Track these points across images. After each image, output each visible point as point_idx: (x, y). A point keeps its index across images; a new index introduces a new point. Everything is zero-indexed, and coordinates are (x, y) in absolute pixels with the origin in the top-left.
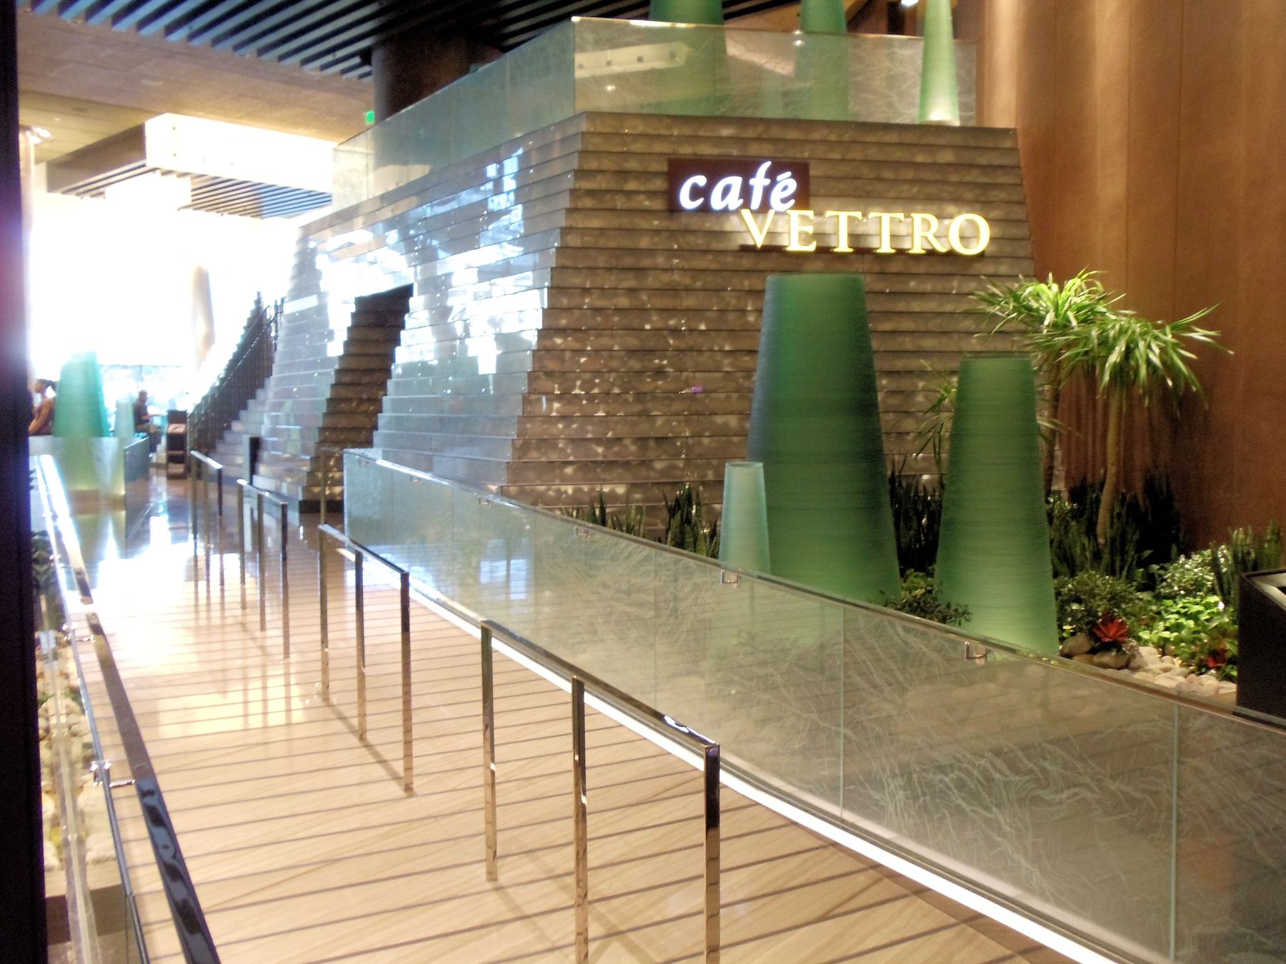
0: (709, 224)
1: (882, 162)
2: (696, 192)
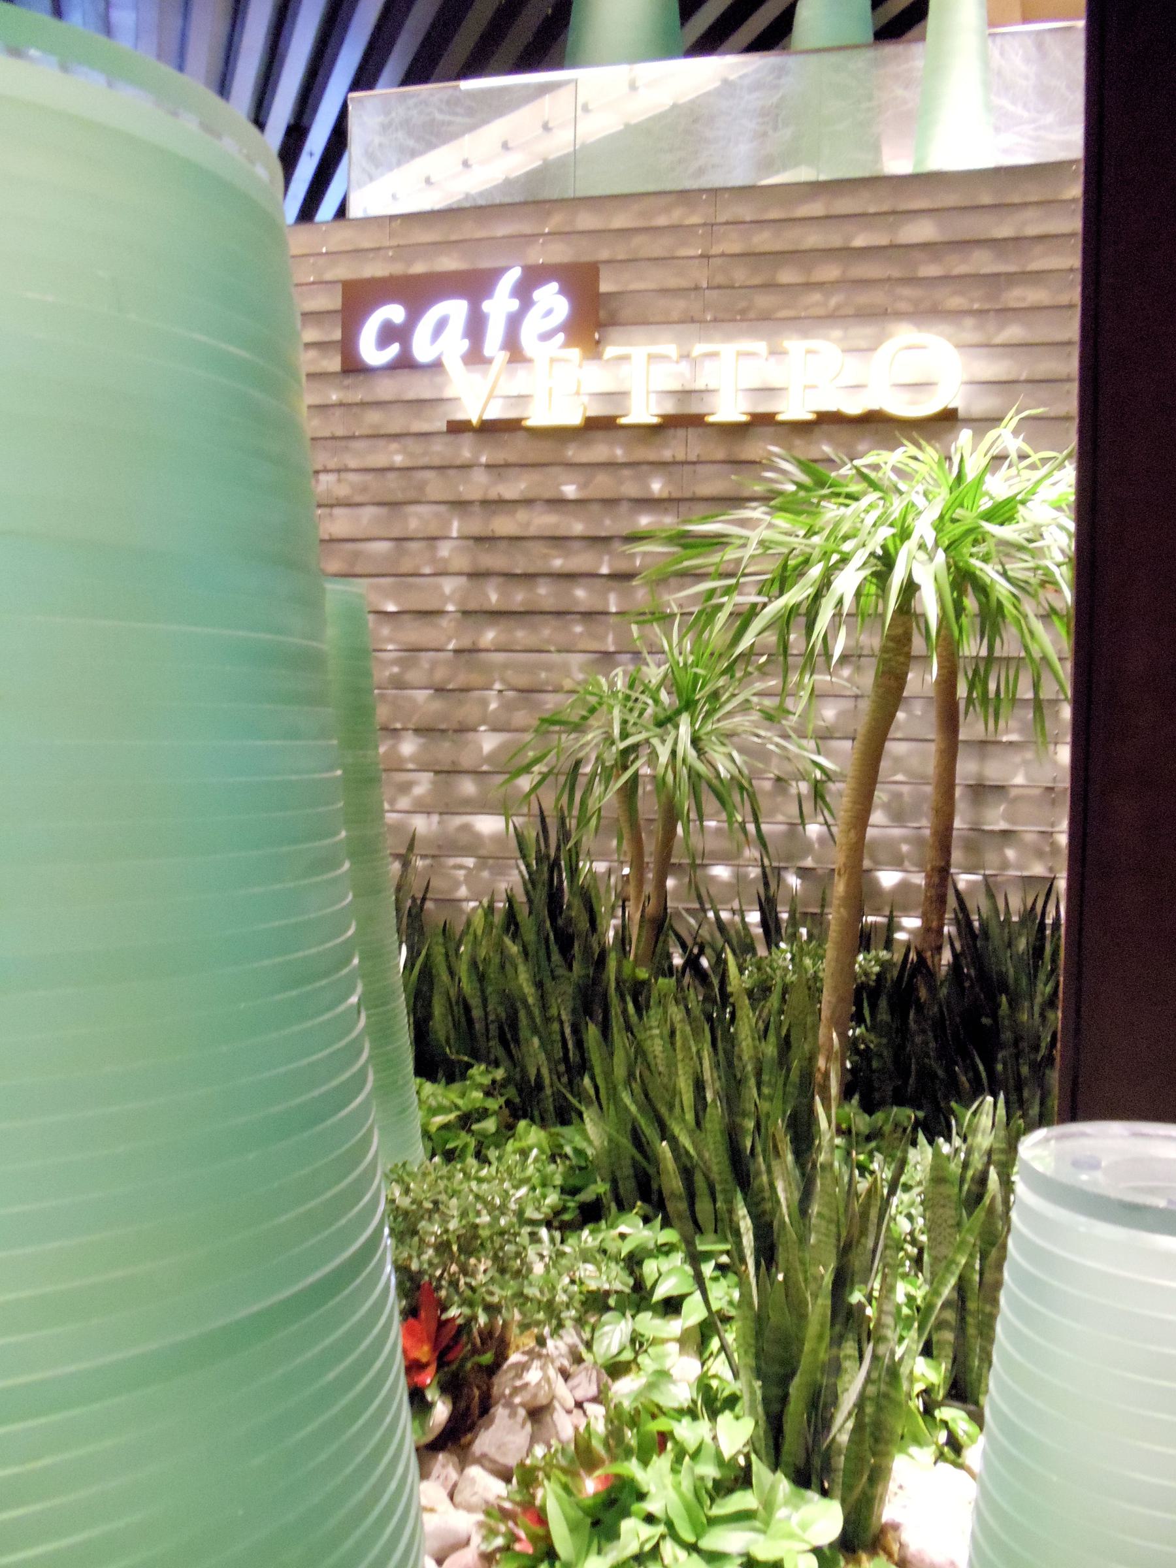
0: (417, 387)
2: (388, 334)
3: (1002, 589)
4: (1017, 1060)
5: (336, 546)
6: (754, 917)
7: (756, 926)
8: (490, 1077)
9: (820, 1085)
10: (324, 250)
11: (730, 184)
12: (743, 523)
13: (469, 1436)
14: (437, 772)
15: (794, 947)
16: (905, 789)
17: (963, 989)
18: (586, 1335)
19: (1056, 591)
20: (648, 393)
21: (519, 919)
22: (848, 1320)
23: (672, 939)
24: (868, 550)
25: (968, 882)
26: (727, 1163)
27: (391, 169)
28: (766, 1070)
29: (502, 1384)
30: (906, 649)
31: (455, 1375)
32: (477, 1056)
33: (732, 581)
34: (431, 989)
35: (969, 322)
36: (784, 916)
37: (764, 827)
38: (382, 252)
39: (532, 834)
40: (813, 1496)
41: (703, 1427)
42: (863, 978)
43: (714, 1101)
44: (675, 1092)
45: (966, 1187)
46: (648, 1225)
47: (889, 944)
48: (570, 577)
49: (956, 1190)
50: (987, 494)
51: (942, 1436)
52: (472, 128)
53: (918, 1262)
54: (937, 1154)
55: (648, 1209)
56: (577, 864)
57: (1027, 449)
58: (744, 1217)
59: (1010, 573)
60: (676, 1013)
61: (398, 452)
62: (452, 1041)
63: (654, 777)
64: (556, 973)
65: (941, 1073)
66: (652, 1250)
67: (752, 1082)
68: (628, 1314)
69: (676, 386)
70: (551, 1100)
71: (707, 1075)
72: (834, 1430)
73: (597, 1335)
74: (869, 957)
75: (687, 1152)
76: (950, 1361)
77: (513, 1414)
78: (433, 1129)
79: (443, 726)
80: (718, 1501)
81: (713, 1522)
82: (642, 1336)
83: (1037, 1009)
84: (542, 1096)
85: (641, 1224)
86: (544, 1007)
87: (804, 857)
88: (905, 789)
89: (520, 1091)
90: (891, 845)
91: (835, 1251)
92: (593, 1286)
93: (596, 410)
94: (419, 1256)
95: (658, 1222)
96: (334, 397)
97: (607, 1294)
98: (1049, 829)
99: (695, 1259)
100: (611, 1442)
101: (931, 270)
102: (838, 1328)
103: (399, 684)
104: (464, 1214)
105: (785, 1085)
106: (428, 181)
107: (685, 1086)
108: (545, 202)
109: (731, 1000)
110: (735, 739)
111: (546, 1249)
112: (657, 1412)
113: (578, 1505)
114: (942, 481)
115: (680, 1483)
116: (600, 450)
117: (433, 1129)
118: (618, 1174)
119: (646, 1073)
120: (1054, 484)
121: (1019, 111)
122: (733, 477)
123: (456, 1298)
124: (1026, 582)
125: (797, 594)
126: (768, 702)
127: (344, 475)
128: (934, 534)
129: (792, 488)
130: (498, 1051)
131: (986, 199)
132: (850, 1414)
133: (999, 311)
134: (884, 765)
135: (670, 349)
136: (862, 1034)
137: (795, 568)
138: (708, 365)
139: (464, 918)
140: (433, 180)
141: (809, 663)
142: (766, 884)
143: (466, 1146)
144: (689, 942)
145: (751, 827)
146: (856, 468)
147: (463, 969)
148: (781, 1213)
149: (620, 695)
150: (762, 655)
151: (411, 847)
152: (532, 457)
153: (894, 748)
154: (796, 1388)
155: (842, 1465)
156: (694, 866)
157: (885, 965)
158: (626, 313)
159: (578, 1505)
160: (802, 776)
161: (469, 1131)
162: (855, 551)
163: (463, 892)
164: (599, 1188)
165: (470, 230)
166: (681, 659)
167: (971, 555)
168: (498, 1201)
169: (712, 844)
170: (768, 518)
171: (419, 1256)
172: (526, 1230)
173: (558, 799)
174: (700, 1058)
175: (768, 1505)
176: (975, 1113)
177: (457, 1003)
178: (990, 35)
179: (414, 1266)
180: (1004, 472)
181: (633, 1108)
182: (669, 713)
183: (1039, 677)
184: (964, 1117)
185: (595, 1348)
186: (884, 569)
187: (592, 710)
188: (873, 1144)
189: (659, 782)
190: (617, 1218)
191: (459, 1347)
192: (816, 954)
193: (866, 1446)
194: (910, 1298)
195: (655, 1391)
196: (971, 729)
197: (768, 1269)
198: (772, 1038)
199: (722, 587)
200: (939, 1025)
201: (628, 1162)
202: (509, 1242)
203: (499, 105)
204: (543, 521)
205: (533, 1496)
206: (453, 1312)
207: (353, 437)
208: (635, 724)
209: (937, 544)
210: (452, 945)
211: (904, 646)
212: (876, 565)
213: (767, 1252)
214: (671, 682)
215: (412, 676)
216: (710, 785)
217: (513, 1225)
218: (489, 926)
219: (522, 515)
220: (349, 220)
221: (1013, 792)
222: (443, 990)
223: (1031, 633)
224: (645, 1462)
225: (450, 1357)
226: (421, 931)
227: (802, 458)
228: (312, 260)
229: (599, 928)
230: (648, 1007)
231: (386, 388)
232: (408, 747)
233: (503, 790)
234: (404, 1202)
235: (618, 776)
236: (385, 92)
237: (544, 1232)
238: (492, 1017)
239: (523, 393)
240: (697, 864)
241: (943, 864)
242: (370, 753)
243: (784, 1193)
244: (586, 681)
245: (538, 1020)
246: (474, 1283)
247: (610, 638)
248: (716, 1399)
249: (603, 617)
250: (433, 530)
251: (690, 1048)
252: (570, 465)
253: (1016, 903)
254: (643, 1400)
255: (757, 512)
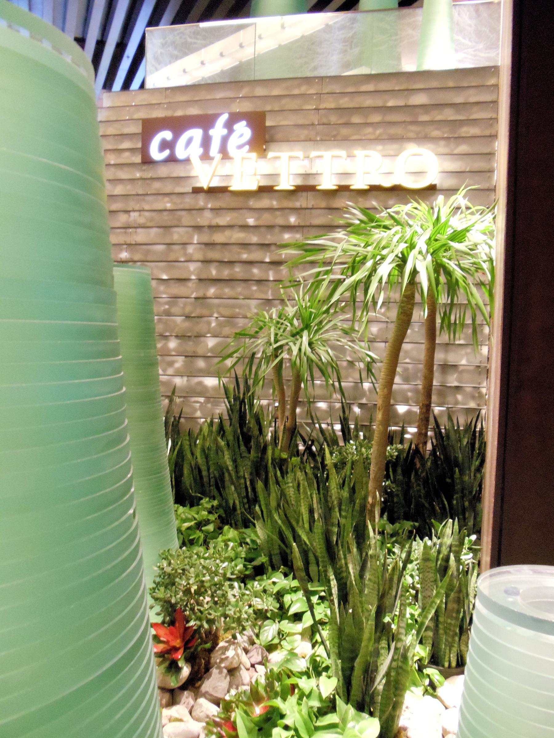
0: (178, 171)
1: (266, 96)
2: (164, 145)
3: (458, 273)
4: (463, 500)
5: (138, 247)
6: (338, 427)
7: (339, 431)
8: (211, 504)
9: (369, 510)
10: (133, 104)
11: (329, 75)
12: (333, 240)
13: (199, 683)
14: (186, 356)
15: (357, 443)
16: (410, 366)
17: (437, 465)
18: (256, 631)
19: (483, 274)
20: (289, 175)
21: (225, 429)
22: (382, 631)
23: (299, 438)
24: (395, 253)
25: (439, 410)
26: (325, 548)
27: (166, 65)
28: (343, 504)
29: (216, 657)
30: (412, 301)
31: (193, 653)
32: (204, 494)
33: (329, 268)
34: (183, 461)
35: (442, 143)
36: (352, 426)
37: (342, 384)
38: (162, 105)
39: (231, 387)
40: (365, 715)
41: (313, 682)
42: (390, 458)
43: (318, 519)
44: (299, 514)
45: (439, 563)
46: (286, 578)
47: (402, 442)
48: (251, 263)
49: (434, 564)
50: (450, 226)
51: (427, 682)
52: (205, 46)
53: (416, 597)
54: (425, 546)
55: (286, 570)
56: (253, 402)
57: (470, 205)
58: (333, 580)
59: (462, 265)
60: (300, 475)
61: (168, 202)
62: (193, 487)
63: (290, 359)
64: (243, 455)
65: (427, 505)
66: (288, 590)
67: (337, 509)
68: (277, 621)
69: (302, 171)
70: (240, 516)
71: (315, 506)
72: (376, 684)
73: (261, 631)
74: (392, 448)
75: (305, 543)
76: (431, 645)
77: (221, 672)
78: (183, 529)
79: (189, 335)
80: (320, 718)
81: (317, 729)
82: (283, 631)
83: (472, 474)
84: (236, 513)
85: (283, 577)
86: (237, 472)
87: (362, 398)
88: (410, 366)
89: (225, 511)
90: (403, 393)
91: (377, 597)
92: (260, 607)
93: (263, 183)
94: (175, 596)
95: (291, 576)
96: (138, 175)
97: (267, 611)
98: (478, 386)
99: (308, 594)
100: (268, 689)
101: (424, 118)
102: (378, 634)
103: (168, 313)
104: (197, 576)
105: (353, 511)
106: (184, 71)
107: (304, 511)
108: (239, 82)
109: (327, 468)
110: (329, 342)
111: (236, 591)
112: (290, 674)
113: (252, 721)
114: (429, 219)
115: (301, 710)
116: (265, 202)
117: (183, 529)
118: (272, 552)
119: (286, 505)
120: (482, 222)
121: (467, 42)
122: (330, 216)
123: (193, 616)
124: (469, 269)
125: (359, 275)
126: (346, 326)
127: (142, 213)
128: (426, 246)
129: (358, 222)
130: (215, 492)
131: (451, 84)
132: (384, 677)
133: (456, 138)
134: (401, 354)
135: (300, 154)
136: (389, 484)
137: (359, 262)
138: (318, 161)
139: (199, 427)
140: (186, 71)
141: (366, 308)
142: (344, 412)
143: (199, 537)
144: (307, 439)
145: (337, 384)
146: (389, 214)
147: (198, 453)
148: (351, 578)
149: (274, 321)
150: (343, 301)
151: (174, 392)
152: (232, 205)
153: (406, 347)
154: (358, 664)
155: (379, 701)
156: (310, 402)
157: (400, 451)
158: (279, 136)
159: (252, 721)
160: (361, 360)
161: (201, 530)
162: (388, 254)
163: (198, 414)
164: (263, 559)
165: (203, 95)
166: (304, 304)
167: (444, 257)
168: (214, 569)
169: (318, 392)
170: (346, 237)
171: (175, 596)
172: (227, 583)
173: (244, 371)
174: (312, 498)
175: (344, 720)
176: (444, 526)
177: (195, 468)
178: (454, 5)
179: (173, 601)
180: (458, 216)
181: (279, 522)
182: (298, 330)
183: (475, 315)
184: (439, 527)
185: (261, 637)
186: (402, 263)
187: (261, 328)
188: (394, 539)
189: (293, 365)
190: (271, 574)
191: (194, 640)
192: (368, 446)
193: (392, 692)
194: (412, 615)
195: (289, 663)
196: (442, 338)
197: (344, 604)
198: (346, 488)
199: (323, 271)
200: (426, 482)
201: (277, 547)
202: (219, 589)
203: (219, 34)
204: (238, 236)
205: (230, 716)
206: (192, 623)
207: (147, 195)
208: (281, 335)
209: (427, 252)
210: (193, 441)
211: (411, 300)
212: (398, 261)
213: (344, 598)
214: (298, 315)
215: (174, 310)
216: (318, 366)
217: (221, 581)
218: (210, 432)
219: (228, 233)
220: (146, 89)
221: (461, 368)
222: (188, 462)
223: (472, 294)
224: (284, 699)
225: (190, 645)
226: (178, 433)
227: (362, 207)
228: (127, 109)
229: (263, 433)
230: (287, 473)
231: (163, 171)
232: (173, 344)
233: (218, 365)
234: (168, 570)
235: (273, 361)
236: (164, 27)
237: (236, 584)
238: (212, 476)
239: (228, 174)
240: (311, 402)
241: (428, 402)
242: (152, 351)
243: (352, 570)
244: (257, 314)
245: (234, 477)
246: (202, 609)
247: (270, 292)
248: (319, 666)
249: (266, 283)
250: (185, 240)
251: (307, 493)
252: (251, 209)
253: (462, 421)
254: (283, 668)
255: (340, 234)
